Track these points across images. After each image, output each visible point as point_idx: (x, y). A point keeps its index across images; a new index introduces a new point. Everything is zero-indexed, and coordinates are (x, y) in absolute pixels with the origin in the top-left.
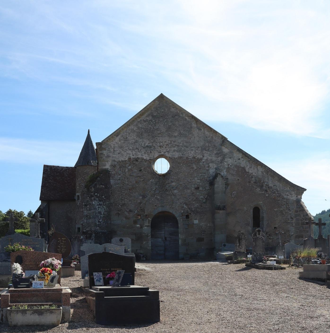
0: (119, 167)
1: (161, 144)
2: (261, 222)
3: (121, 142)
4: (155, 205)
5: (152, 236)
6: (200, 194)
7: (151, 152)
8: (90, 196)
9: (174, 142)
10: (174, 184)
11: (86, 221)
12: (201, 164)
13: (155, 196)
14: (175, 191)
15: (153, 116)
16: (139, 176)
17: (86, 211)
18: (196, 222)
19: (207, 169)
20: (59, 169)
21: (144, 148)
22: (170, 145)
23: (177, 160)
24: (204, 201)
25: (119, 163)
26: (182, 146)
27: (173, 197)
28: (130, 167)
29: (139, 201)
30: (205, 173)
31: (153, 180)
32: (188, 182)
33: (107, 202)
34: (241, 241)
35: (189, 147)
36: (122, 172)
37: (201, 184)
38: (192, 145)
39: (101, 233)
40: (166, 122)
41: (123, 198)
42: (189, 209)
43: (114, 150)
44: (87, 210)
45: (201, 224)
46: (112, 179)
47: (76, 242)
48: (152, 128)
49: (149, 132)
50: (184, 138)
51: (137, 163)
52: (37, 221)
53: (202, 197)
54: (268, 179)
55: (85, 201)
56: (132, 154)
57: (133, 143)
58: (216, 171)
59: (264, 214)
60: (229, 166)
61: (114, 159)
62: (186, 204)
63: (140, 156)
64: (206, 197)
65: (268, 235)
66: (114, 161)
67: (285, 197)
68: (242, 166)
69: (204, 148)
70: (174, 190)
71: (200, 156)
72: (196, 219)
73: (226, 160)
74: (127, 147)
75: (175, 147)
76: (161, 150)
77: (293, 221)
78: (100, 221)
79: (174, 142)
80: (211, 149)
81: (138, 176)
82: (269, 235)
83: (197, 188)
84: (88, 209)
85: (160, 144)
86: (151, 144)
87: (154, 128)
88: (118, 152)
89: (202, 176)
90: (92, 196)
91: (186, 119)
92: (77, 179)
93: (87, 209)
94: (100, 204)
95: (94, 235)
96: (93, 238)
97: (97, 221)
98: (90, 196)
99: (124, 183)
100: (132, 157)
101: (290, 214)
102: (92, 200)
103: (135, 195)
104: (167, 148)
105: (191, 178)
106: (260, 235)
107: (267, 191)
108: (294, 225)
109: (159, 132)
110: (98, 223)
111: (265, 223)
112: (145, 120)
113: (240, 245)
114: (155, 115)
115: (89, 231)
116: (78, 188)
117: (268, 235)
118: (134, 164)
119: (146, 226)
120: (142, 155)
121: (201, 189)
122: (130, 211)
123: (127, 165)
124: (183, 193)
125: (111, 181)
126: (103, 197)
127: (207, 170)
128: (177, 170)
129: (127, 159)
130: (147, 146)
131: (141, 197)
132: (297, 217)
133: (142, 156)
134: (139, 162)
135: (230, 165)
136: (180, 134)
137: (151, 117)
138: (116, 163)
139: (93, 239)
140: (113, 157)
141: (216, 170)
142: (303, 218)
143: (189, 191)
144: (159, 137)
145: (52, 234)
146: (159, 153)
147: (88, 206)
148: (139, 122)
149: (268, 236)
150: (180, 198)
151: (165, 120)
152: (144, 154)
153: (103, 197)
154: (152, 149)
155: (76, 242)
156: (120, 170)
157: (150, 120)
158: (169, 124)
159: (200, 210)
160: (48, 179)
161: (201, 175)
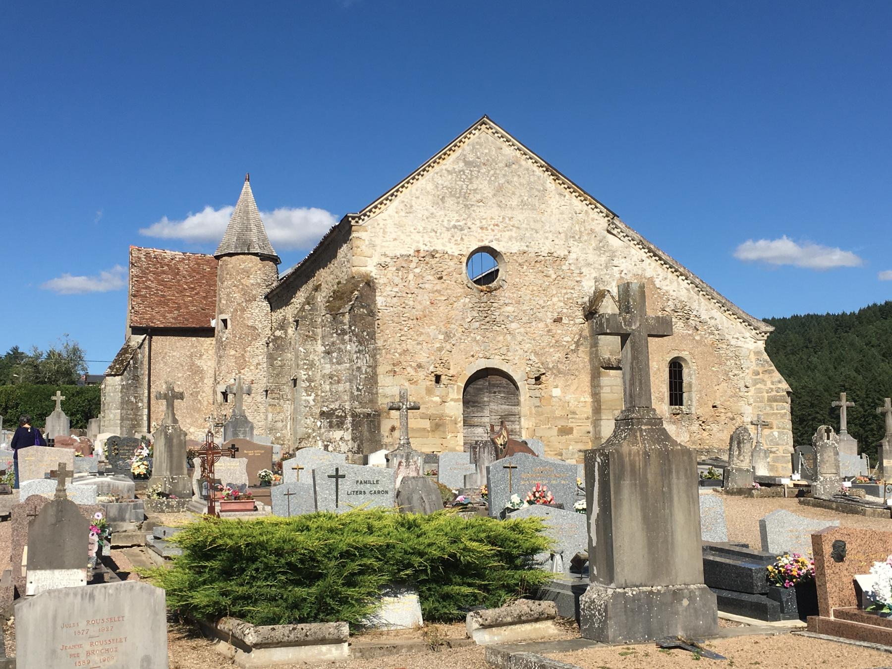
0: (395, 269)
1: (484, 222)
2: (685, 395)
3: (400, 214)
4: (472, 353)
5: (467, 423)
6: (564, 332)
7: (462, 239)
8: (339, 332)
9: (510, 220)
10: (509, 309)
11: (328, 387)
12: (564, 267)
13: (472, 335)
14: (514, 326)
15: (468, 163)
16: (436, 291)
17: (328, 366)
18: (556, 392)
19: (578, 279)
20: (166, 258)
21: (448, 229)
22: (501, 226)
23: (515, 257)
24: (573, 347)
25: (395, 260)
26: (527, 229)
27: (509, 337)
28: (417, 270)
29: (438, 346)
30: (573, 289)
31: (467, 300)
32: (538, 307)
33: (372, 346)
34: (742, 445)
35: (541, 233)
36: (402, 279)
37: (565, 311)
38: (547, 228)
39: (362, 416)
40: (493, 175)
41: (402, 338)
42: (542, 364)
43: (384, 231)
44: (332, 363)
45: (567, 398)
46: (380, 294)
47: (486, 454)
48: (465, 186)
49: (458, 195)
50: (530, 212)
51: (433, 262)
52: (404, 407)
53: (568, 339)
54: (699, 303)
55: (327, 343)
56: (424, 241)
57: (424, 217)
58: (597, 283)
59: (693, 377)
60: (623, 275)
61: (383, 250)
62: (536, 354)
63: (439, 248)
64: (575, 340)
65: (701, 422)
66: (385, 255)
67: (733, 342)
68: (648, 275)
69: (571, 236)
70: (512, 322)
71: (562, 253)
72: (556, 387)
73: (615, 262)
74: (413, 226)
75: (511, 230)
76: (483, 235)
77: (749, 394)
78: (360, 387)
79: (511, 219)
80: (585, 238)
81: (435, 289)
82: (703, 422)
83: (558, 320)
84: (335, 360)
85: (481, 222)
86: (464, 222)
87: (469, 187)
88: (394, 236)
89: (566, 293)
90: (344, 332)
91: (533, 171)
92: (222, 283)
93: (331, 360)
94: (359, 350)
95: (349, 419)
96: (349, 425)
97: (355, 387)
98: (339, 332)
99: (404, 303)
100: (422, 248)
101: (743, 378)
102: (343, 342)
103: (429, 330)
104: (496, 231)
105: (545, 299)
106: (831, 439)
107: (698, 330)
108: (751, 401)
109: (479, 197)
110: (356, 393)
111: (695, 396)
112: (449, 169)
113: (739, 454)
114: (471, 159)
115: (336, 409)
116: (224, 302)
117: (701, 422)
118: (427, 263)
119: (452, 400)
120: (444, 245)
121: (566, 322)
122: (420, 366)
123: (413, 265)
124: (528, 329)
125: (377, 298)
126: (365, 333)
127: (577, 282)
128: (517, 280)
129: (412, 252)
130: (455, 227)
131: (441, 337)
132: (758, 386)
133: (444, 248)
134: (437, 259)
135: (625, 272)
136: (523, 204)
137: (463, 164)
138: (388, 260)
139: (347, 430)
140: (382, 247)
141: (595, 282)
142: (772, 386)
143: (541, 325)
144: (478, 206)
145: (504, 445)
146: (479, 241)
147: (335, 355)
148: (437, 173)
149: (700, 425)
150: (523, 340)
151: (492, 172)
152: (447, 244)
153: (365, 333)
154: (465, 232)
155: (486, 454)
156: (398, 276)
157: (460, 172)
158: (500, 182)
159: (564, 368)
160: (144, 279)
161: (565, 291)
